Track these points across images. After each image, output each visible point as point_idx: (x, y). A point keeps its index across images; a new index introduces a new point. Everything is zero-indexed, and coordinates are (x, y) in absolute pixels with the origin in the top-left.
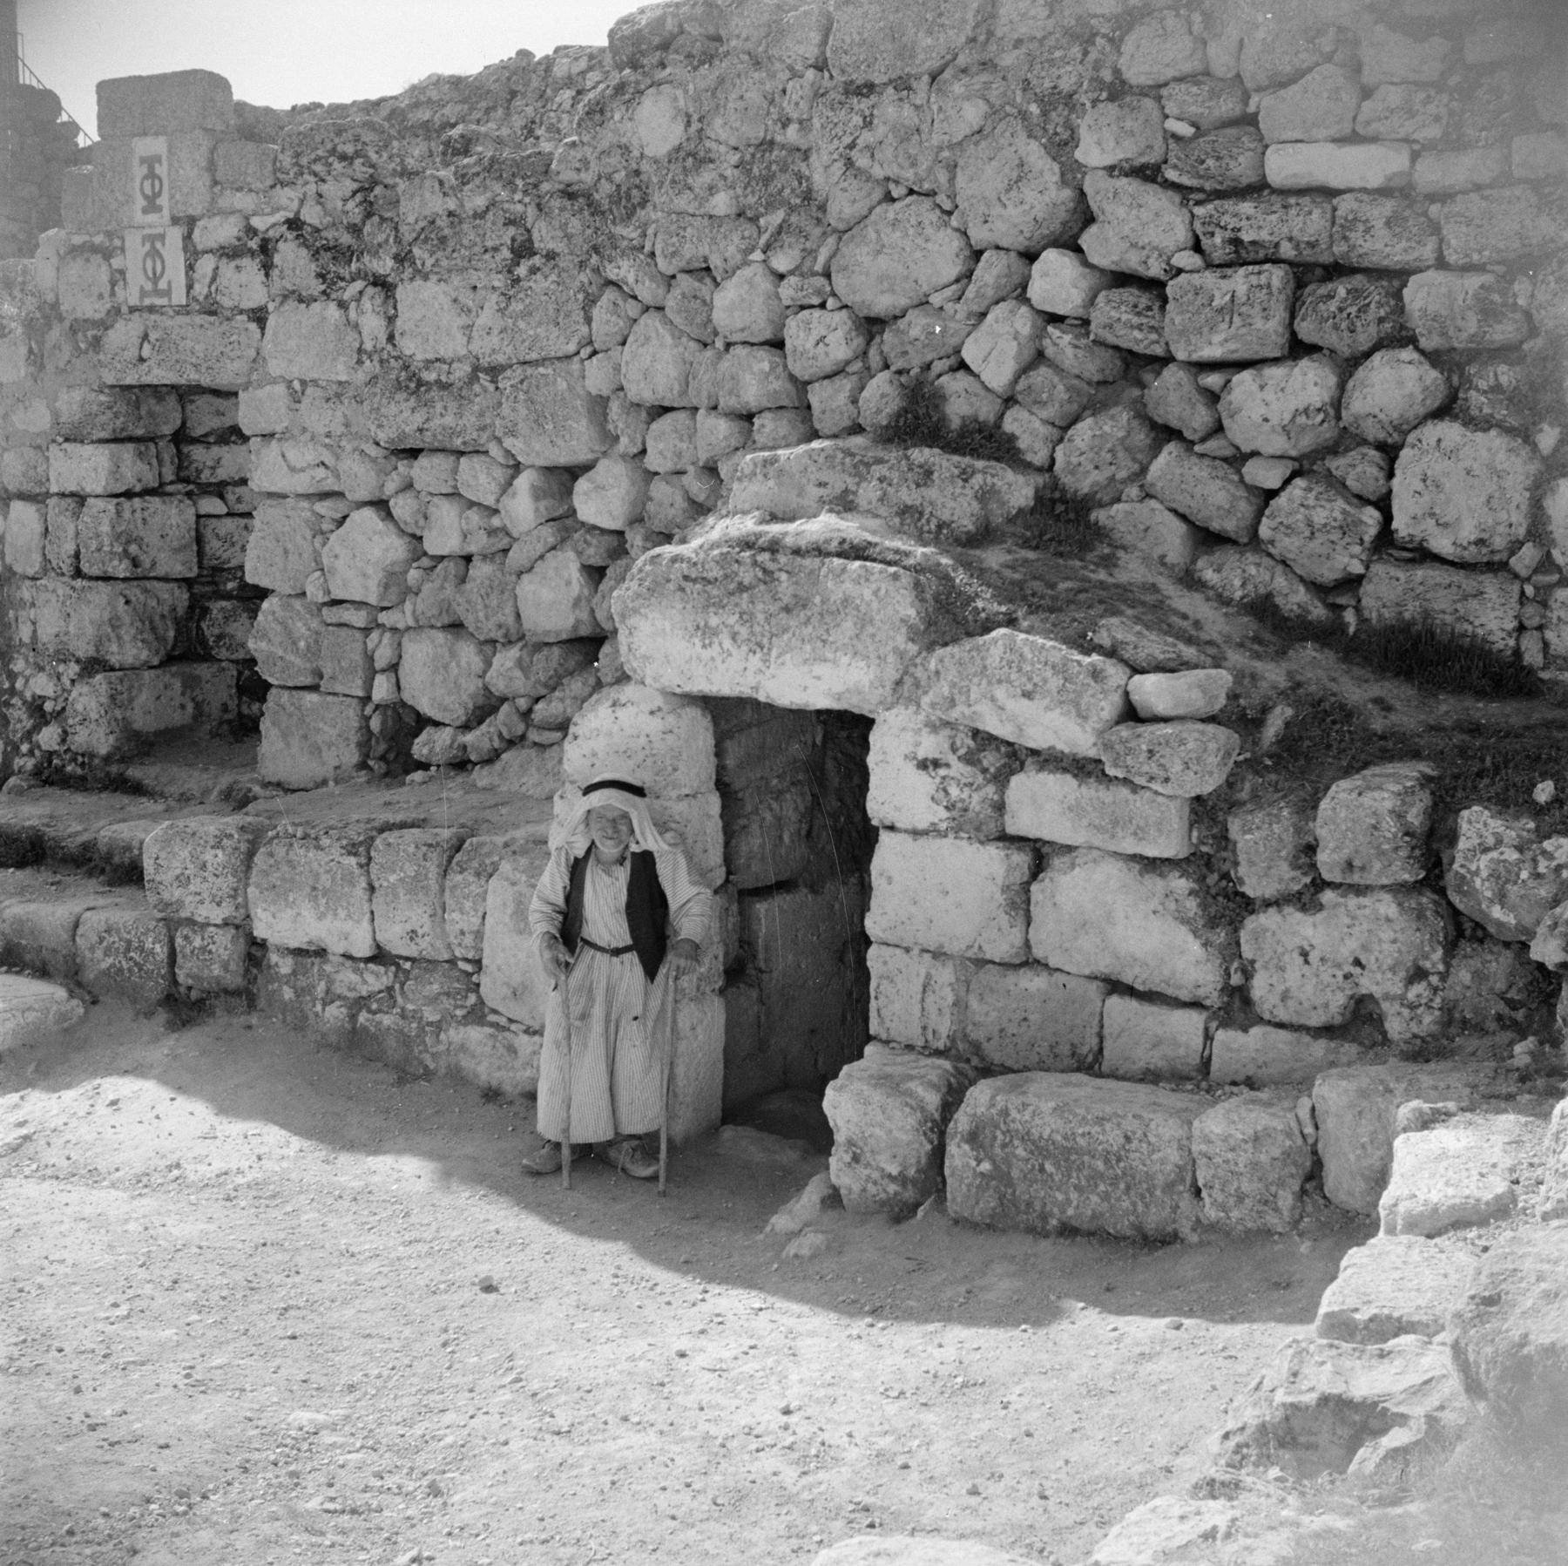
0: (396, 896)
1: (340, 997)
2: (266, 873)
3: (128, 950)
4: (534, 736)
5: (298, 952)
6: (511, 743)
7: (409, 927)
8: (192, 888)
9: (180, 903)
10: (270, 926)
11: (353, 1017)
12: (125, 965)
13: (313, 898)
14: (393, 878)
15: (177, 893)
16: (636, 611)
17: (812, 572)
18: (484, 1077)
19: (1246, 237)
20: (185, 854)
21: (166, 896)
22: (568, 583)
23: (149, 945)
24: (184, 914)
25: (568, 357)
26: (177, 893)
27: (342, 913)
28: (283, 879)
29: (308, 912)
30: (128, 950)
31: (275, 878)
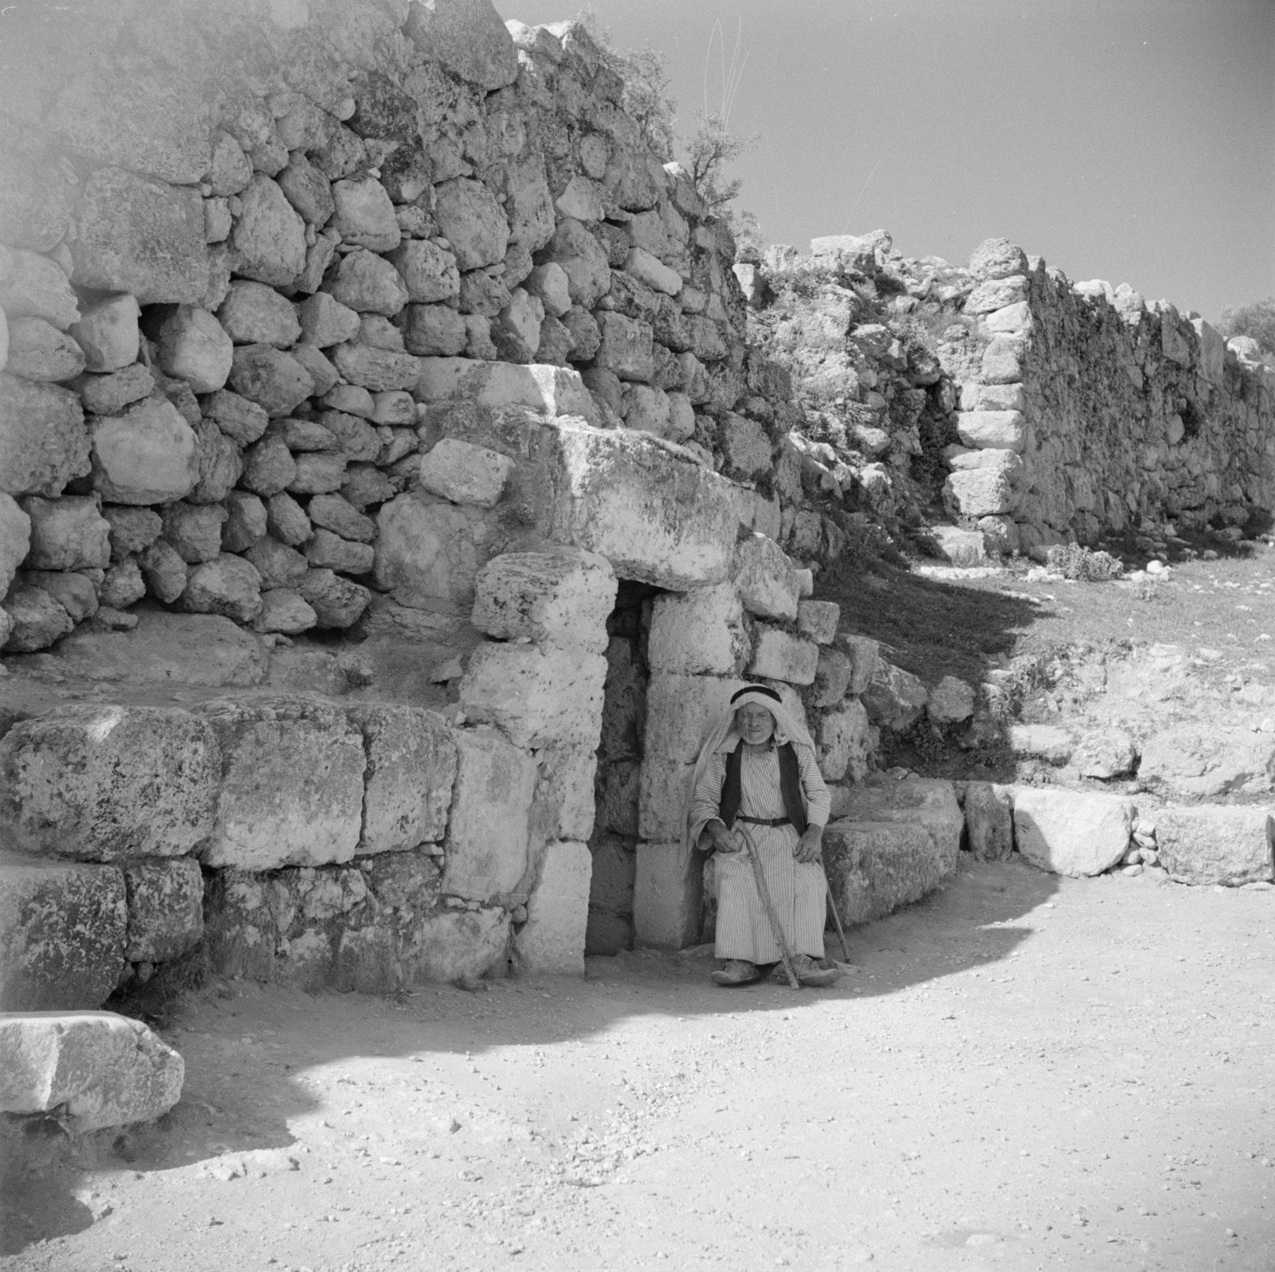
0: (395, 777)
1: (314, 921)
2: (249, 770)
3: (73, 921)
4: (112, 617)
5: (272, 875)
6: (86, 623)
7: (400, 814)
8: (161, 804)
9: (144, 830)
10: (241, 846)
11: (334, 942)
12: (65, 949)
13: (304, 796)
14: (395, 756)
15: (141, 815)
16: (610, 485)
17: (690, 474)
18: (449, 970)
19: (637, 300)
20: (156, 753)
21: (125, 823)
22: (179, 439)
23: (107, 906)
24: (147, 847)
25: (191, 186)
26: (141, 815)
27: (336, 808)
28: (273, 775)
29: (295, 816)
30: (73, 921)
31: (261, 775)
